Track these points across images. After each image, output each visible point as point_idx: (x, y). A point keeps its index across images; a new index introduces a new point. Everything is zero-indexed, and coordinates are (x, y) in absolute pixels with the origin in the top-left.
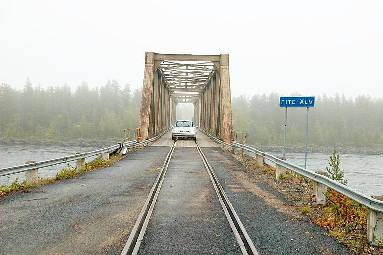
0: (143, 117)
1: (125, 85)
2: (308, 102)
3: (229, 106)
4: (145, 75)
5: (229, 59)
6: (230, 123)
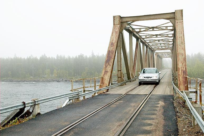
0: (106, 67)
3: (183, 53)
4: (113, 33)
5: (182, 14)
6: (184, 69)
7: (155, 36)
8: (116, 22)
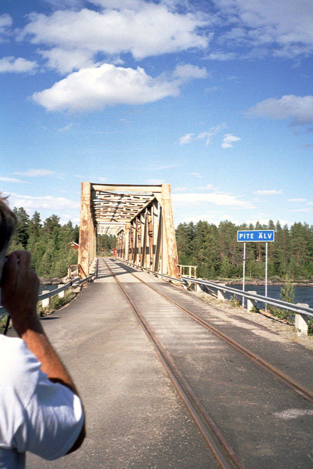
1: (34, 214)
2: (267, 236)
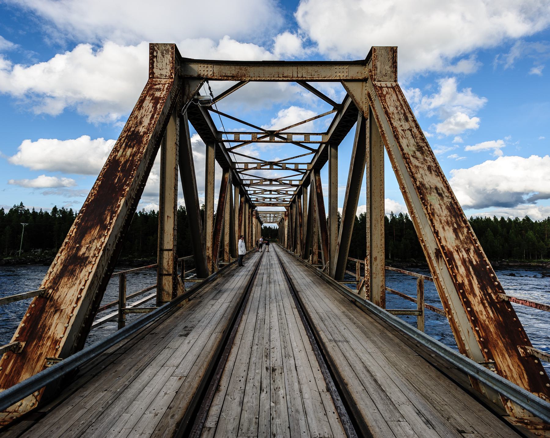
4: (142, 101)
7: (269, 193)
8: (160, 66)
